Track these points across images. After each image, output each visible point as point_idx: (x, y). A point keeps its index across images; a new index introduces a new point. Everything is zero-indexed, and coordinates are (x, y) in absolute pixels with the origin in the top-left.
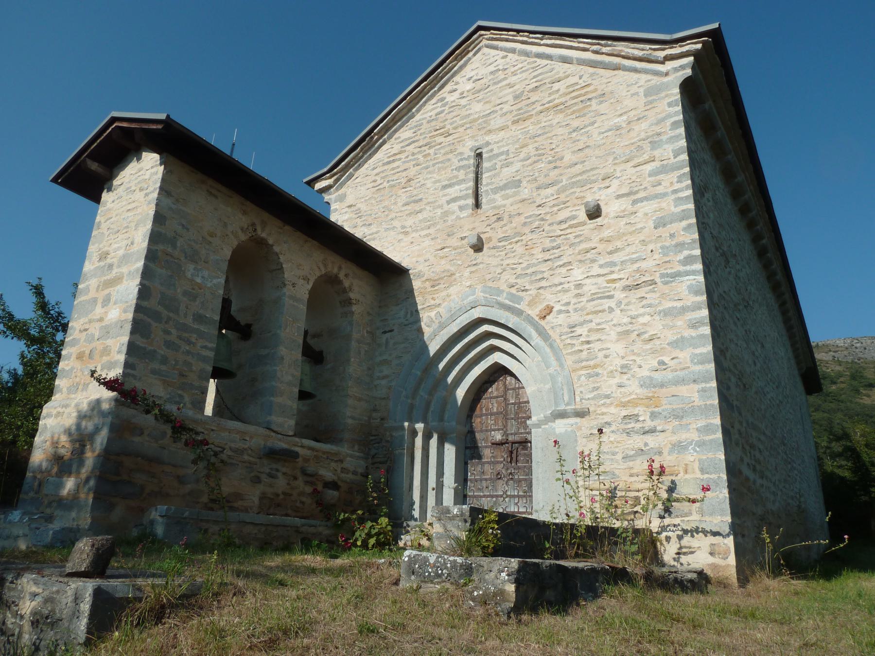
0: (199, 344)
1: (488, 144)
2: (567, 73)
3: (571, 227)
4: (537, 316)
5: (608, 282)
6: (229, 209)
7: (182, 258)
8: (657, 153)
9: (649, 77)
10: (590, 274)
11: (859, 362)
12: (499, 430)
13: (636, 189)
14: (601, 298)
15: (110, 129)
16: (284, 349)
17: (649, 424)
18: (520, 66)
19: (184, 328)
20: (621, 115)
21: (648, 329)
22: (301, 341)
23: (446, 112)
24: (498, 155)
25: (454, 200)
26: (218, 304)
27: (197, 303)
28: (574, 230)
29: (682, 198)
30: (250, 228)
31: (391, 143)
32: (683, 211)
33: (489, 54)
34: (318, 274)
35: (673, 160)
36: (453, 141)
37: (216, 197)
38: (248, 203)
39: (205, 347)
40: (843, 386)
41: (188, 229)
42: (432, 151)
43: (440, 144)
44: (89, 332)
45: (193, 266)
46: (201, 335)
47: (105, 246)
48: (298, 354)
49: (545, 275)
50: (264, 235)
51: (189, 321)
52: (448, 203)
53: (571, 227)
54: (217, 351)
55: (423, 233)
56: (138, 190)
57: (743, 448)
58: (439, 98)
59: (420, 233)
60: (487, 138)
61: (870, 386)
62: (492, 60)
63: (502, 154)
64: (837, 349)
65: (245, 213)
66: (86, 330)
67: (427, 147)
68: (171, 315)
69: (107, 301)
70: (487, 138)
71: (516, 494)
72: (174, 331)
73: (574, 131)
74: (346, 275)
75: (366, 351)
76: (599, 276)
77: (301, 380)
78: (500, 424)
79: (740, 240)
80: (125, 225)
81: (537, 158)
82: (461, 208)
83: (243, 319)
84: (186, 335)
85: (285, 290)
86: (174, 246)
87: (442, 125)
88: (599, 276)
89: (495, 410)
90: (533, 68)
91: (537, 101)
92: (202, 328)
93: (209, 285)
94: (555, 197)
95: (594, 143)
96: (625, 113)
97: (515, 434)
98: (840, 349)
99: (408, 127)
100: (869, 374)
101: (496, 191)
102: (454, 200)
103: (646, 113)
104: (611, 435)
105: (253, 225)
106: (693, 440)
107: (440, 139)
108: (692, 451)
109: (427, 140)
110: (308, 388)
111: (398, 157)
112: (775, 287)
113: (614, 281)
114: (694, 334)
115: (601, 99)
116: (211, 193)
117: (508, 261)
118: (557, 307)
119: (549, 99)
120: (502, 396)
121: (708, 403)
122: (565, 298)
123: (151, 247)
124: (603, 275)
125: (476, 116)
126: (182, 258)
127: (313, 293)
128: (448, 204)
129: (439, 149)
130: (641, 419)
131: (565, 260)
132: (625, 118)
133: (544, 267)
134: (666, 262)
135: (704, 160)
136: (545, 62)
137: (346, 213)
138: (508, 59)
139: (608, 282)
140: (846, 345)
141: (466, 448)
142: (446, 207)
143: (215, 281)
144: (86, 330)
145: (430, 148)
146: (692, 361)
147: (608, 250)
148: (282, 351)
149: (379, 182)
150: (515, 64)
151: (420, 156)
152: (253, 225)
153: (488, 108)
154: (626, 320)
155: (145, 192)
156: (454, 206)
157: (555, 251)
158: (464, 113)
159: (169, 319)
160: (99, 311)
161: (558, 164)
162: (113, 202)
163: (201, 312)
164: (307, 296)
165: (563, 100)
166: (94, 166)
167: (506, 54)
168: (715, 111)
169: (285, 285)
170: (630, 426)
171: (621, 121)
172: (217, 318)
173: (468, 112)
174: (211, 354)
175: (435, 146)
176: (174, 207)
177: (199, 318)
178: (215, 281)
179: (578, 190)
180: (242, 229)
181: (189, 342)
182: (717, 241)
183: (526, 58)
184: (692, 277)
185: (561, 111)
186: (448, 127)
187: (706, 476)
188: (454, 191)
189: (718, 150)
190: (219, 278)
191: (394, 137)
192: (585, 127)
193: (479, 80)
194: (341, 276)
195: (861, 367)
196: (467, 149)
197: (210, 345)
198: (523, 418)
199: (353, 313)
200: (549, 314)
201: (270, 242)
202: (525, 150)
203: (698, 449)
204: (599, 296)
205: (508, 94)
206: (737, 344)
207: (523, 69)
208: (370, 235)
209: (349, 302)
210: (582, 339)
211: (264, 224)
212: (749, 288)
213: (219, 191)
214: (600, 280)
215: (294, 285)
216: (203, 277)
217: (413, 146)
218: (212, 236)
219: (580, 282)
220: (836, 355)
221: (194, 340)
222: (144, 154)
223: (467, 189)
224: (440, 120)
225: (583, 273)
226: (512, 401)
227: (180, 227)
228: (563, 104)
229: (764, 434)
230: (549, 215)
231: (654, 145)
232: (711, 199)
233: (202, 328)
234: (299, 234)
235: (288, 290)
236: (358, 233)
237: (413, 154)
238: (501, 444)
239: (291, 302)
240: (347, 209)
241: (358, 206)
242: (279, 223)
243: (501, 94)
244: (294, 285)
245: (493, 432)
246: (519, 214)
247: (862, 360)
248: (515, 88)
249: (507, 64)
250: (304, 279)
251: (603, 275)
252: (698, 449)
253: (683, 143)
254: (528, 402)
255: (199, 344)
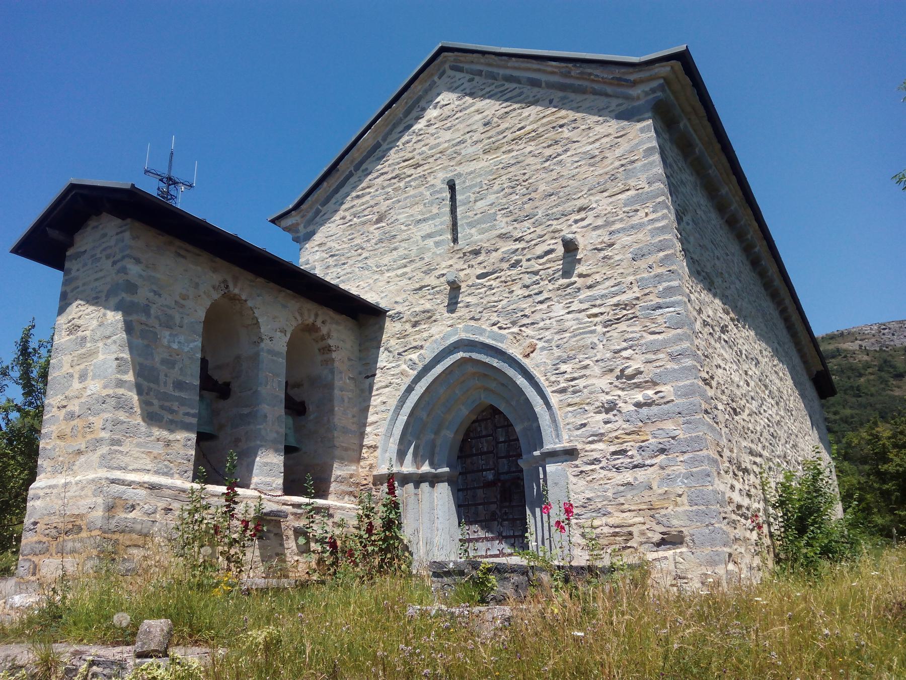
0: (181, 412)
1: (459, 175)
2: (536, 98)
3: (549, 261)
4: (521, 354)
5: (589, 316)
6: (199, 268)
7: (157, 326)
8: (632, 182)
9: (620, 101)
10: (570, 309)
11: (887, 350)
12: (490, 470)
13: (612, 219)
14: (581, 334)
15: (70, 196)
16: (266, 406)
17: (638, 460)
18: (488, 89)
19: (165, 397)
20: (594, 142)
21: (630, 363)
22: (283, 396)
23: (414, 141)
24: (471, 187)
25: (429, 236)
26: (196, 369)
27: (176, 370)
28: (552, 264)
29: (658, 228)
30: (222, 285)
31: (358, 175)
32: (660, 241)
33: (455, 77)
34: (295, 324)
35: (647, 189)
36: (424, 173)
37: (184, 257)
38: (218, 259)
39: (187, 414)
40: (872, 377)
41: (160, 295)
42: (402, 184)
43: (410, 176)
44: (68, 409)
45: (169, 333)
46: (183, 402)
47: (74, 319)
48: (281, 410)
49: (527, 312)
50: (236, 291)
51: (170, 389)
52: (424, 238)
53: (549, 261)
54: (199, 416)
55: (400, 272)
56: (104, 258)
57: (735, 474)
58: (405, 125)
59: (396, 272)
60: (459, 169)
61: (899, 376)
62: (460, 83)
63: (475, 186)
64: (864, 337)
65: (215, 270)
66: (65, 407)
67: (397, 179)
68: (152, 385)
69: (83, 377)
70: (459, 169)
71: (512, 534)
72: (155, 402)
73: (547, 160)
74: (323, 322)
75: (349, 399)
76: (580, 311)
77: (286, 434)
78: (491, 463)
79: (727, 255)
80: (94, 296)
81: (511, 190)
82: (437, 244)
83: (220, 377)
84: (167, 404)
85: (263, 345)
86: (148, 314)
87: (410, 155)
88: (580, 311)
89: (485, 449)
90: (501, 92)
91: (507, 129)
92: (183, 395)
93: (186, 349)
94: (532, 230)
95: (568, 172)
96: (597, 140)
97: (507, 473)
98: (868, 336)
99: (376, 157)
100: (899, 362)
101: (471, 225)
102: (429, 236)
103: (619, 140)
104: (602, 471)
105: (225, 281)
106: (680, 473)
107: (409, 171)
108: (680, 484)
109: (397, 172)
110: (293, 443)
111: (368, 190)
112: (774, 296)
113: (596, 315)
114: (676, 367)
115: (573, 125)
116: (179, 255)
117: (487, 299)
118: (540, 344)
119: (520, 126)
120: (491, 435)
121: (693, 435)
122: (548, 334)
123: (127, 318)
124: (584, 310)
125: (446, 145)
126: (157, 326)
127: (290, 344)
128: (423, 241)
129: (410, 182)
130: (629, 453)
131: (545, 295)
132: (597, 145)
133: (524, 305)
134: (645, 295)
135: (682, 182)
136: (514, 85)
137: (317, 251)
138: (474, 83)
139: (589, 316)
140: (873, 332)
141: (459, 490)
142: (421, 244)
143: (192, 345)
144: (65, 407)
145: (401, 180)
146: (675, 394)
147: (588, 284)
148: (265, 408)
149: (348, 218)
150: (483, 87)
151: (389, 189)
152: (225, 281)
153: (457, 136)
154: (609, 355)
155: (112, 260)
156: (430, 242)
157: (535, 286)
158: (432, 142)
159: (150, 389)
160: (76, 385)
161: (533, 195)
162: (78, 270)
163: (180, 378)
164: (286, 349)
165: (535, 126)
166: (54, 234)
167: (472, 76)
168: (691, 129)
169: (262, 340)
170: (619, 461)
171: (593, 149)
172: (197, 382)
173: (437, 141)
174: (194, 421)
175: (405, 178)
176: (144, 274)
177: (179, 385)
178: (192, 345)
179: (555, 222)
180: (214, 288)
181: (171, 411)
182: (699, 264)
183: (493, 81)
184: (672, 309)
185: (533, 139)
186: (417, 157)
187: (695, 508)
188: (427, 228)
189: (698, 167)
190: (195, 341)
191: (361, 169)
192: (559, 155)
193: (446, 105)
194: (319, 323)
195: (891, 355)
196: (439, 180)
197: (193, 411)
198: (514, 456)
199: (333, 360)
200: (532, 352)
201: (244, 298)
202: (498, 182)
203: (686, 481)
204: (581, 331)
205: (477, 121)
206: (725, 369)
207: (492, 93)
208: (345, 275)
209: (328, 349)
210: (567, 376)
211: (236, 279)
212: (739, 304)
213: (187, 250)
214: (581, 315)
215: (271, 339)
216: (179, 342)
217: (382, 178)
218: (184, 299)
219: (562, 317)
220: (864, 344)
221: (176, 408)
222: (104, 213)
223: (441, 224)
224: (409, 149)
225: (564, 308)
226: (502, 439)
227: (152, 294)
228: (534, 131)
229: (761, 456)
230: (527, 250)
231: (629, 174)
232: (691, 223)
233: (183, 395)
234: (272, 285)
235: (265, 345)
236: (330, 278)
237: (383, 188)
238: (492, 484)
239: (270, 357)
240: (317, 248)
241: (329, 244)
242: (250, 276)
243: (470, 122)
244: (271, 339)
245: (484, 473)
246: (496, 250)
247: (890, 348)
248: (484, 114)
249: (475, 87)
250: (281, 331)
251: (584, 310)
252: (686, 481)
253: (659, 170)
254: (517, 440)
255: (181, 412)
